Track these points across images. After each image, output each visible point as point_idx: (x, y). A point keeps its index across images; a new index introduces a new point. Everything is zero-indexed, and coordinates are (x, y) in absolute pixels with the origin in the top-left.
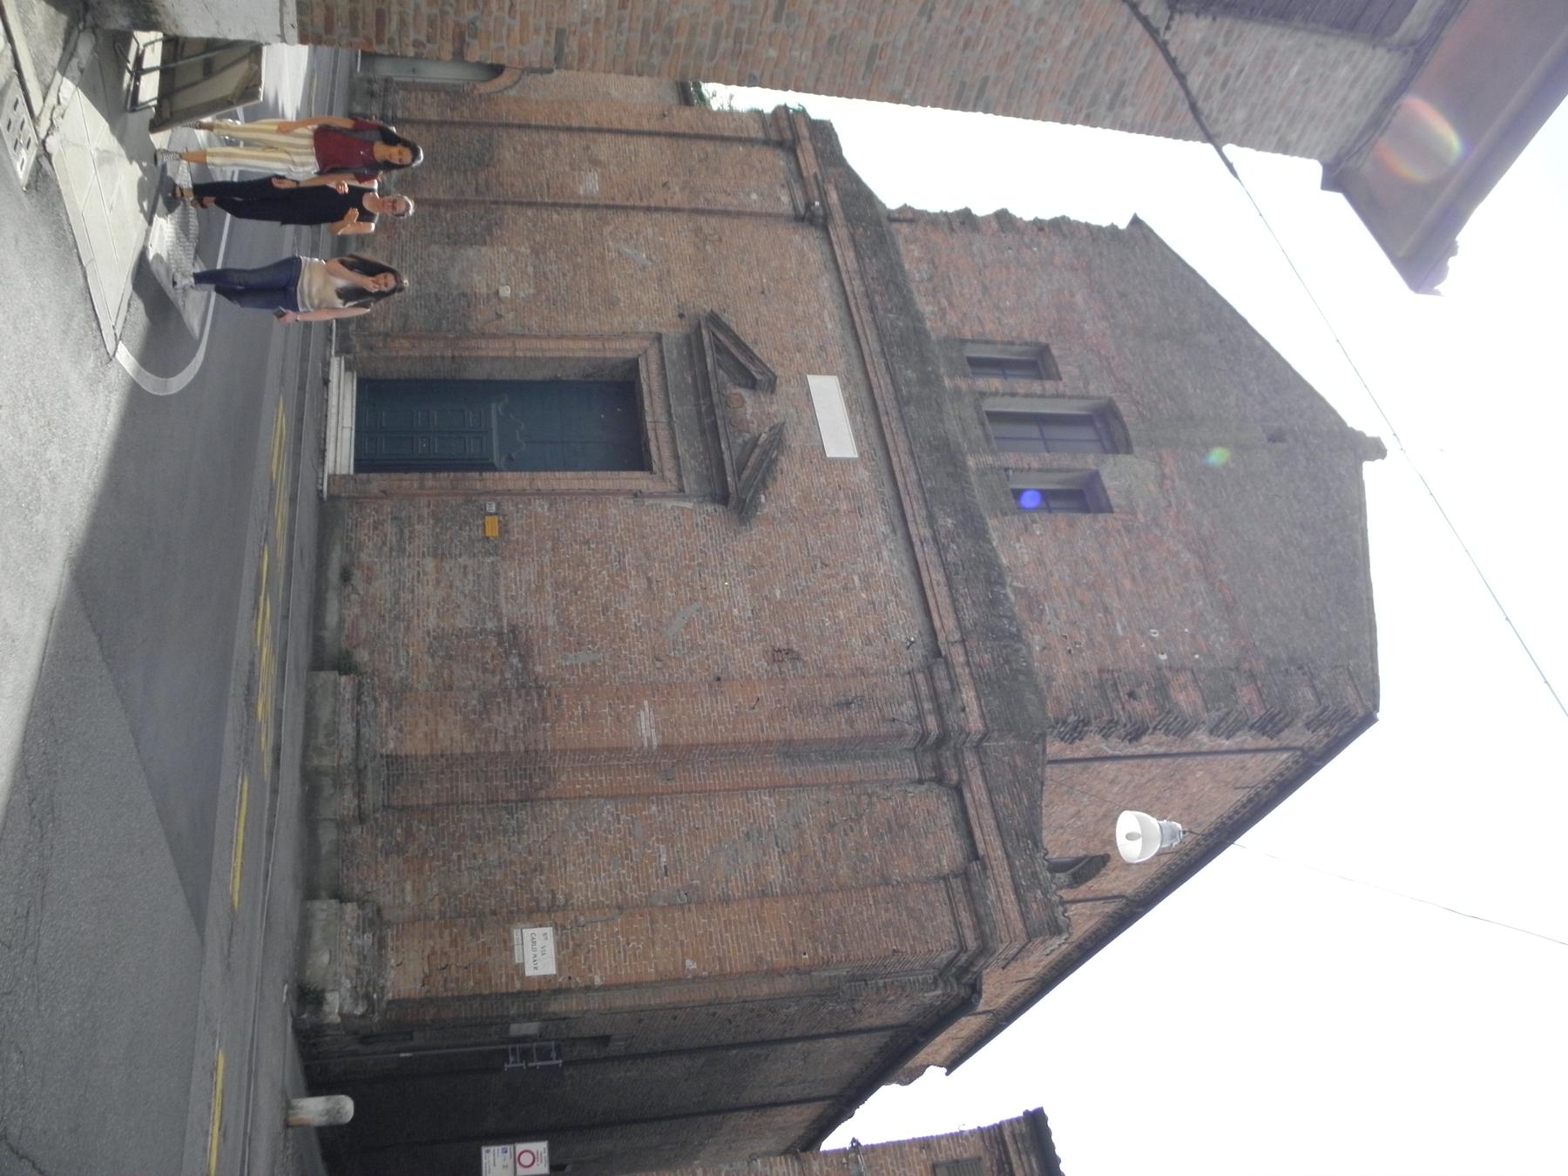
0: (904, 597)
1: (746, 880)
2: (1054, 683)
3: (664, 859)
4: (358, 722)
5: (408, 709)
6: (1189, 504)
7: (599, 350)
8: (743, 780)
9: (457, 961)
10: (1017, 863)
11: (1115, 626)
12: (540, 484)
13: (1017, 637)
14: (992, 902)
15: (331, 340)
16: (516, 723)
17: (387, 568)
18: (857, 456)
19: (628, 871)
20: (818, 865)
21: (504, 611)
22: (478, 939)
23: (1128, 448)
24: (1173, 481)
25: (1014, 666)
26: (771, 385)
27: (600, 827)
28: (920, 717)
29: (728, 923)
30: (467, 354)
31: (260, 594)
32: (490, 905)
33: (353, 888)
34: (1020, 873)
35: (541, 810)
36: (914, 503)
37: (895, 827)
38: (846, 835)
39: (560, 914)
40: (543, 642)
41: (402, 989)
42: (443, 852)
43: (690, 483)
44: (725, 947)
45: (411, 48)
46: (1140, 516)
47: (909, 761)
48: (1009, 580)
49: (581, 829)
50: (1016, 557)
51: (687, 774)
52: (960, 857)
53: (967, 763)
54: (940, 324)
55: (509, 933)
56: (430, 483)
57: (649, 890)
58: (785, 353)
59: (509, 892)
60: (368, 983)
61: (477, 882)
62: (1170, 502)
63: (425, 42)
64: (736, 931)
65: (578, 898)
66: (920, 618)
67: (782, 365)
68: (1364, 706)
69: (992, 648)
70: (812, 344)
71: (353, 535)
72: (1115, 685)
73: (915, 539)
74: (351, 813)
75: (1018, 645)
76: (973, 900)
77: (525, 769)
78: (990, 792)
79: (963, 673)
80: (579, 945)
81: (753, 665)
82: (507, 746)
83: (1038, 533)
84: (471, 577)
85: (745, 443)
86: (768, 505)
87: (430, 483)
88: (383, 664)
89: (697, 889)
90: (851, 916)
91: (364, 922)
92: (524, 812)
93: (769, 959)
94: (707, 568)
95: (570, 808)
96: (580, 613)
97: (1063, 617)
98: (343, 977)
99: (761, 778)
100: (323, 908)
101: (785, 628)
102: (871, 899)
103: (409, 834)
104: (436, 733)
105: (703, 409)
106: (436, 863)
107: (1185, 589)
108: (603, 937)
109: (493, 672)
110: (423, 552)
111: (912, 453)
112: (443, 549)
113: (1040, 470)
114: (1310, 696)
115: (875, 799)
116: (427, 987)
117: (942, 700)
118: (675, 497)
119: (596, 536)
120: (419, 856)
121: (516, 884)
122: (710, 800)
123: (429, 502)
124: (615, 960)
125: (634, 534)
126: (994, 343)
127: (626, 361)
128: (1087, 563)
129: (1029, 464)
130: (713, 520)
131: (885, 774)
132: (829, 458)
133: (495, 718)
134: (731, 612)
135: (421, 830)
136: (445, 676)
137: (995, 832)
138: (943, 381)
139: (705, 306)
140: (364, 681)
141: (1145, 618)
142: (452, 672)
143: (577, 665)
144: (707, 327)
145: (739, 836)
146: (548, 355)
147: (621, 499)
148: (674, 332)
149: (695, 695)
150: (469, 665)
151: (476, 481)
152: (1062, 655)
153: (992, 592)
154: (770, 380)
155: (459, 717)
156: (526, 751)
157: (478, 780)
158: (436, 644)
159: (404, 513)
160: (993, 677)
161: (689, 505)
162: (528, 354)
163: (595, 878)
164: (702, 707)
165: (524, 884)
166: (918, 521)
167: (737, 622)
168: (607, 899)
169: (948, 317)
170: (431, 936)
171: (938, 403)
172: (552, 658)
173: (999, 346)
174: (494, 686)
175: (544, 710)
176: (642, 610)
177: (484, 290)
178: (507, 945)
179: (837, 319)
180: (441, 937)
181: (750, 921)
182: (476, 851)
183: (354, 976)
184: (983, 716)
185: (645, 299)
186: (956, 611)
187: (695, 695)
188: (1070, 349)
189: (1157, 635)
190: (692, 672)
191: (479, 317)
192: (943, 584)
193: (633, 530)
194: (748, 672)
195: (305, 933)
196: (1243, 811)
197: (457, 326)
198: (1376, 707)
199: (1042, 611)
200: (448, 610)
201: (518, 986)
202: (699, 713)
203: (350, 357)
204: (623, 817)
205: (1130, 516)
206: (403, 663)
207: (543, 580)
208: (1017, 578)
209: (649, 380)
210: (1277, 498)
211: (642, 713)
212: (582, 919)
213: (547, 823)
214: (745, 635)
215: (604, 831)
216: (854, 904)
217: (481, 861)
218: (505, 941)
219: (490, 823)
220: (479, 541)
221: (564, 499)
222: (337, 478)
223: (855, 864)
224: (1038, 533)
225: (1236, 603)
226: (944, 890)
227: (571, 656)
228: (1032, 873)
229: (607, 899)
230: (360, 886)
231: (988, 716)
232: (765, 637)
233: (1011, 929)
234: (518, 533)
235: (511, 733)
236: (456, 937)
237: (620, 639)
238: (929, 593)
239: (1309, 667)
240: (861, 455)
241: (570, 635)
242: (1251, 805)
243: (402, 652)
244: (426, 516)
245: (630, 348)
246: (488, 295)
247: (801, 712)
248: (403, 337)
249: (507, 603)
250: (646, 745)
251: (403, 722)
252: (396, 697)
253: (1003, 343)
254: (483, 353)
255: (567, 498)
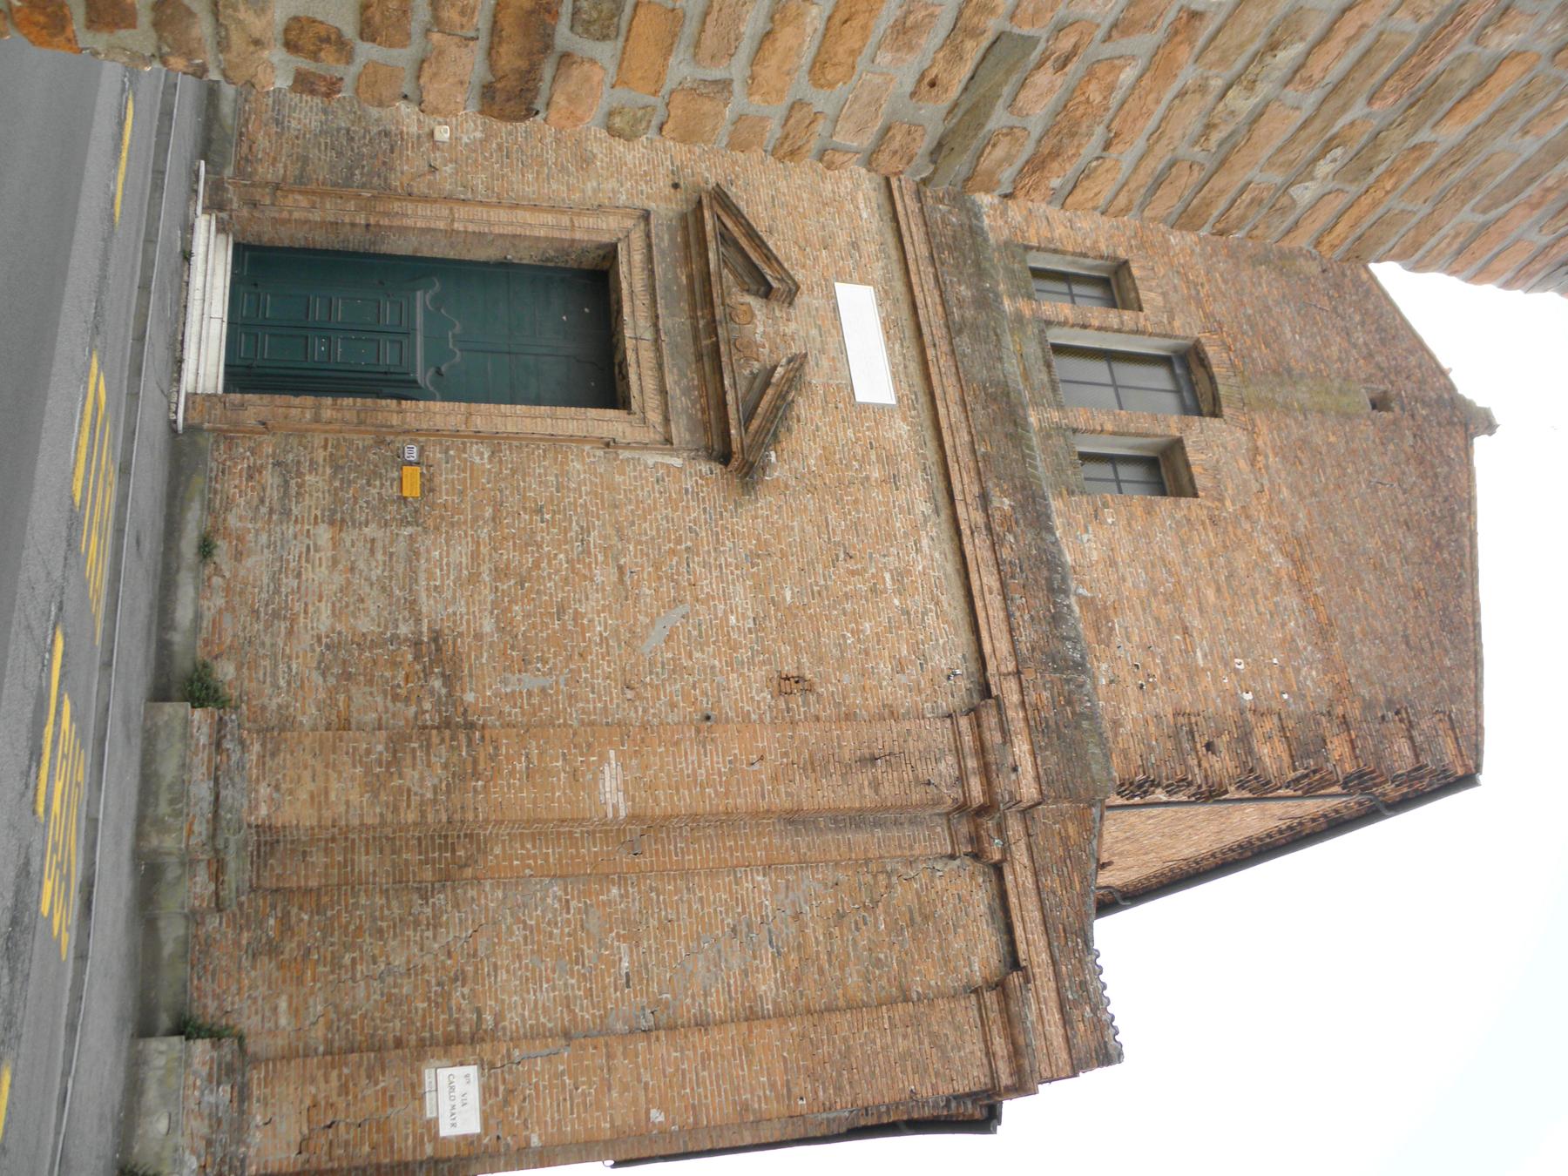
0: (946, 605)
1: (729, 992)
2: (1121, 730)
3: (625, 964)
4: (216, 780)
5: (288, 756)
6: (1284, 489)
7: (566, 228)
8: (732, 855)
9: (347, 1116)
10: (1064, 968)
11: (1195, 653)
12: (479, 422)
13: (1080, 667)
14: (1032, 1023)
15: (196, 192)
16: (436, 781)
17: (264, 538)
18: (894, 402)
19: (579, 982)
20: (821, 971)
21: (424, 610)
22: (376, 1084)
23: (1216, 413)
24: (1266, 457)
25: (1078, 709)
26: (791, 293)
27: (544, 917)
28: (962, 779)
29: (706, 1058)
30: (385, 222)
31: (43, 726)
32: (394, 1029)
33: (205, 1007)
34: (1067, 983)
35: (465, 893)
36: (964, 475)
37: (918, 919)
38: (857, 929)
39: (487, 1046)
40: (477, 658)
41: (270, 1158)
42: (332, 952)
43: (679, 431)
44: (701, 1090)
45: (276, 54)
46: (1228, 503)
47: (941, 830)
48: (1073, 585)
49: (518, 921)
50: (1083, 554)
51: (660, 846)
52: (994, 960)
53: (1010, 833)
54: (1001, 222)
55: (419, 1074)
56: (327, 414)
57: (605, 1008)
58: (808, 249)
59: (420, 1012)
60: (223, 1161)
61: (377, 997)
62: (1262, 485)
63: (350, 31)
64: (716, 1068)
65: (512, 1020)
66: (964, 637)
67: (803, 267)
68: (1465, 765)
69: (1052, 682)
70: (842, 239)
71: (218, 486)
72: (1191, 732)
73: (964, 526)
74: (205, 905)
75: (1082, 678)
76: (1011, 1023)
77: (446, 837)
78: (1036, 874)
79: (1015, 715)
80: (512, 1091)
81: (752, 698)
82: (423, 814)
83: (1110, 521)
84: (380, 556)
85: (754, 376)
86: (779, 468)
87: (327, 414)
88: (254, 684)
89: (667, 1005)
90: (861, 1045)
91: (219, 1065)
92: (442, 896)
93: (756, 1106)
94: (698, 555)
95: (504, 889)
96: (527, 616)
97: (1136, 639)
98: (187, 1152)
99: (755, 852)
100: (163, 1050)
101: (796, 644)
102: (886, 1020)
103: (285, 925)
104: (327, 793)
105: (702, 323)
106: (321, 969)
107: (1276, 605)
108: (544, 1080)
109: (407, 700)
110: (316, 517)
111: (964, 404)
112: (343, 512)
113: (1114, 433)
114: (1407, 752)
115: (894, 879)
116: (305, 1156)
117: (991, 758)
118: (659, 449)
119: (552, 500)
120: (299, 959)
121: (429, 999)
122: (688, 880)
123: (326, 440)
124: (558, 1111)
125: (602, 501)
126: (1064, 253)
127: (600, 246)
128: (1165, 566)
129: (1101, 425)
130: (707, 485)
131: (911, 847)
132: (860, 404)
133: (408, 771)
134: (727, 620)
135: (302, 920)
136: (341, 704)
137: (1041, 928)
138: (1002, 303)
139: (706, 174)
140: (227, 718)
141: (1230, 644)
142: (350, 698)
143: (521, 693)
144: (712, 207)
145: (723, 932)
146: (496, 230)
147: (587, 448)
148: (666, 208)
149: (676, 744)
150: (374, 689)
151: (390, 412)
152: (1132, 692)
153: (1055, 604)
154: (790, 290)
155: (359, 770)
156: (449, 822)
157: (381, 853)
158: (329, 655)
159: (290, 456)
160: (1051, 723)
161: (677, 462)
162: (471, 228)
163: (535, 992)
164: (686, 759)
165: (440, 1000)
166: (969, 501)
167: (734, 636)
168: (549, 1021)
169: (1010, 213)
170: (313, 1080)
171: (997, 335)
172: (487, 680)
173: (1069, 258)
174: (407, 720)
175: (475, 762)
176: (611, 613)
177: (414, 129)
178: (416, 1092)
179: (874, 205)
180: (327, 1082)
181: (734, 1055)
182: (377, 952)
183: (203, 1152)
184: (1038, 778)
185: (629, 158)
186: (1011, 630)
187: (676, 744)
188: (1153, 269)
189: (1242, 667)
190: (673, 705)
191: (406, 168)
192: (995, 592)
193: (602, 494)
194: (747, 708)
195: (133, 1088)
196: (1278, 837)
197: (375, 180)
198: (1478, 768)
199: (1112, 629)
200: (347, 606)
201: (429, 1150)
202: (681, 769)
203: (224, 215)
204: (573, 904)
205: (1217, 503)
206: (282, 683)
207: (479, 565)
208: (1082, 582)
209: (631, 277)
210: (1380, 486)
211: (606, 768)
212: (516, 1053)
213: (473, 911)
214: (744, 654)
215: (549, 924)
216: (866, 1029)
217: (383, 967)
218: (413, 1086)
219: (396, 911)
220: (394, 501)
221: (510, 445)
222: (198, 399)
223: (867, 968)
224: (1110, 521)
225: (1331, 625)
226: (975, 1008)
227: (514, 678)
228: (1081, 982)
229: (549, 1021)
230: (216, 1003)
231: (1043, 781)
232: (769, 659)
233: (1053, 1060)
234: (447, 495)
235: (429, 795)
236: (346, 1082)
237: (581, 655)
238: (979, 604)
239: (1407, 713)
240: (899, 400)
241: (512, 648)
242: (1289, 833)
243: (282, 667)
244: (321, 461)
245: (605, 228)
246: (419, 137)
247: (814, 771)
248: (300, 192)
249: (428, 597)
250: (610, 815)
251: (280, 776)
252: (272, 738)
253: (1074, 254)
254: (409, 222)
255: (515, 443)
